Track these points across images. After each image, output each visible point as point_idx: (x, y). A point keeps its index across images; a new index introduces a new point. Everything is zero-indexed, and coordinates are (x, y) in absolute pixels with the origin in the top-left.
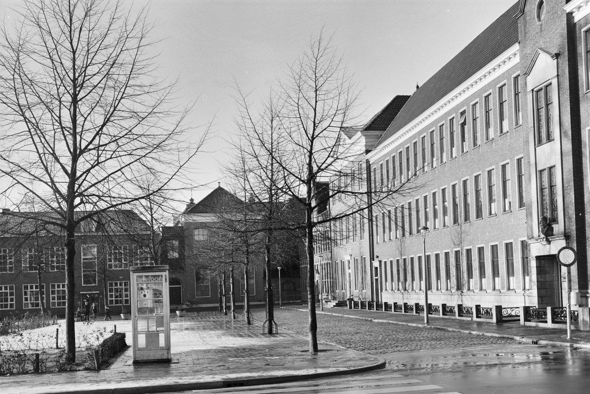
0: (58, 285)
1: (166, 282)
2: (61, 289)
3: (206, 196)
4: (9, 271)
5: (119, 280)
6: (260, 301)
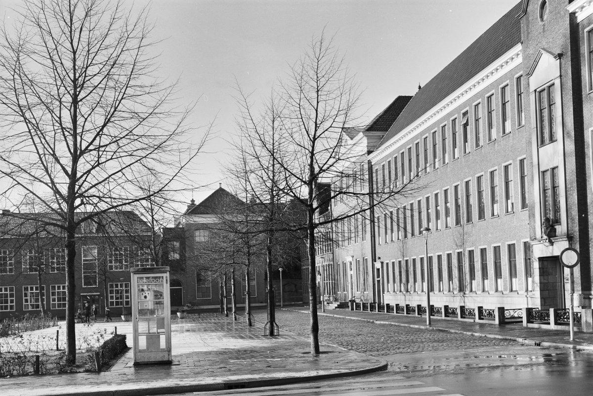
0: (58, 286)
1: (167, 283)
2: (62, 290)
3: (207, 197)
5: (120, 281)
6: (262, 303)
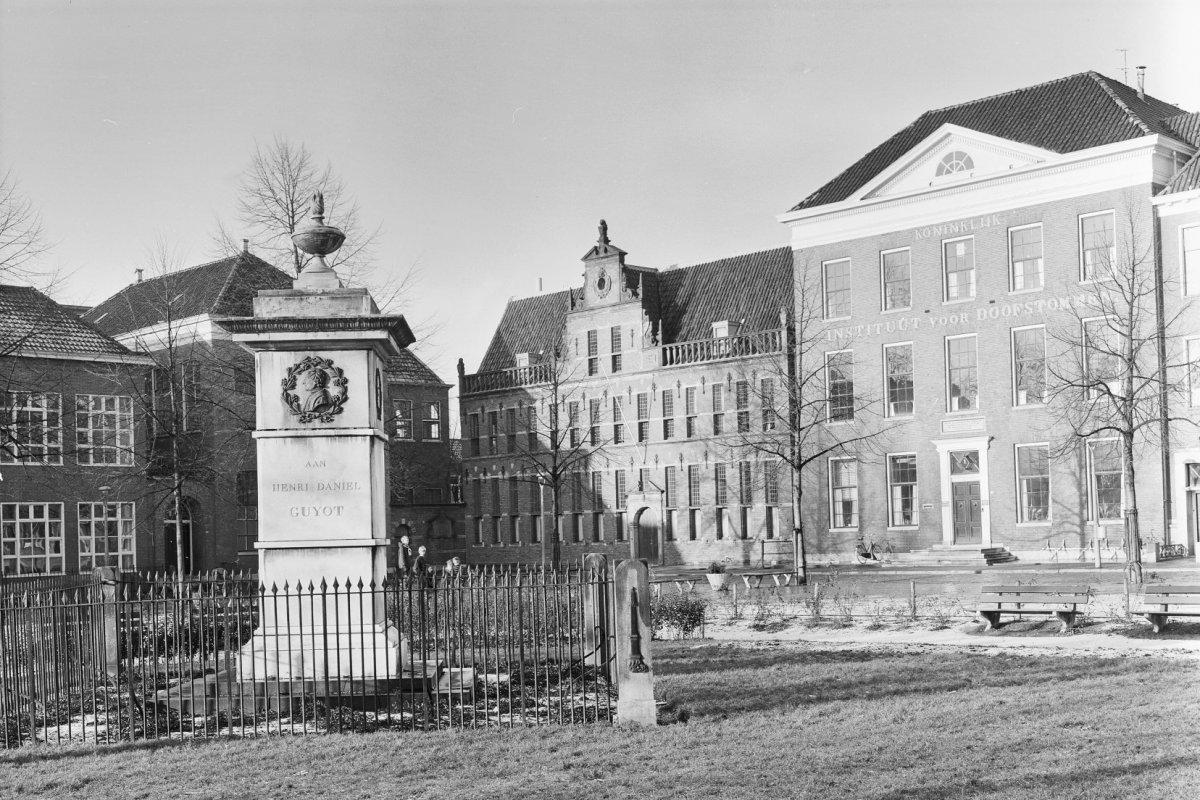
2: (32, 519)
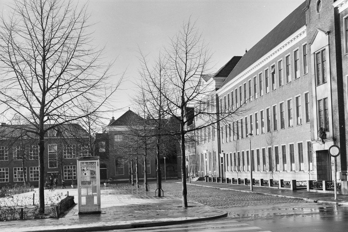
0: (34, 168)
1: (98, 166)
2: (36, 170)
3: (121, 115)
4: (6, 160)
5: (70, 165)
6: (154, 177)
